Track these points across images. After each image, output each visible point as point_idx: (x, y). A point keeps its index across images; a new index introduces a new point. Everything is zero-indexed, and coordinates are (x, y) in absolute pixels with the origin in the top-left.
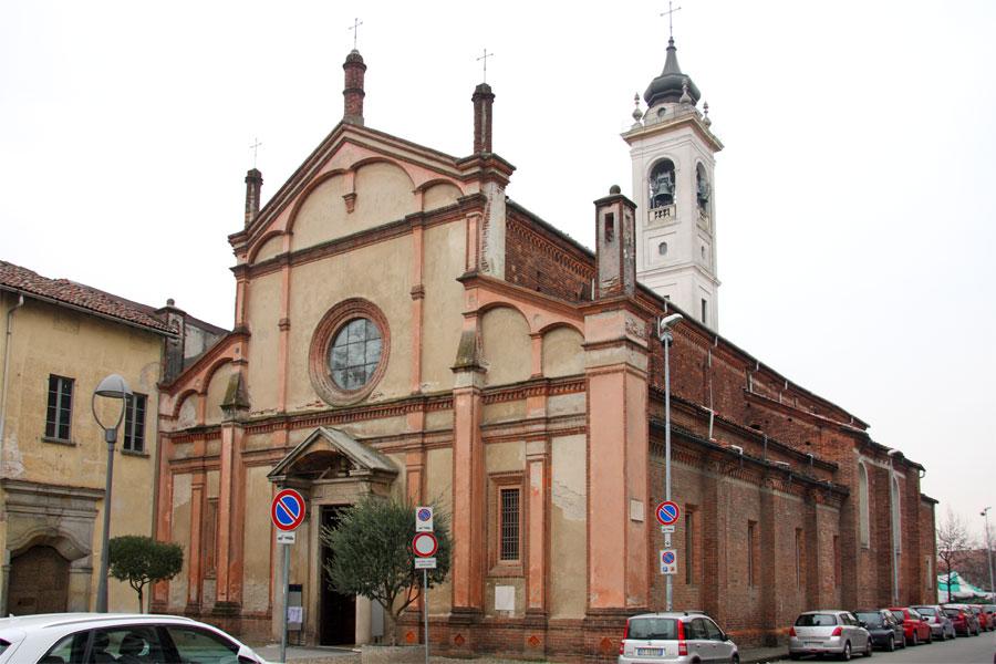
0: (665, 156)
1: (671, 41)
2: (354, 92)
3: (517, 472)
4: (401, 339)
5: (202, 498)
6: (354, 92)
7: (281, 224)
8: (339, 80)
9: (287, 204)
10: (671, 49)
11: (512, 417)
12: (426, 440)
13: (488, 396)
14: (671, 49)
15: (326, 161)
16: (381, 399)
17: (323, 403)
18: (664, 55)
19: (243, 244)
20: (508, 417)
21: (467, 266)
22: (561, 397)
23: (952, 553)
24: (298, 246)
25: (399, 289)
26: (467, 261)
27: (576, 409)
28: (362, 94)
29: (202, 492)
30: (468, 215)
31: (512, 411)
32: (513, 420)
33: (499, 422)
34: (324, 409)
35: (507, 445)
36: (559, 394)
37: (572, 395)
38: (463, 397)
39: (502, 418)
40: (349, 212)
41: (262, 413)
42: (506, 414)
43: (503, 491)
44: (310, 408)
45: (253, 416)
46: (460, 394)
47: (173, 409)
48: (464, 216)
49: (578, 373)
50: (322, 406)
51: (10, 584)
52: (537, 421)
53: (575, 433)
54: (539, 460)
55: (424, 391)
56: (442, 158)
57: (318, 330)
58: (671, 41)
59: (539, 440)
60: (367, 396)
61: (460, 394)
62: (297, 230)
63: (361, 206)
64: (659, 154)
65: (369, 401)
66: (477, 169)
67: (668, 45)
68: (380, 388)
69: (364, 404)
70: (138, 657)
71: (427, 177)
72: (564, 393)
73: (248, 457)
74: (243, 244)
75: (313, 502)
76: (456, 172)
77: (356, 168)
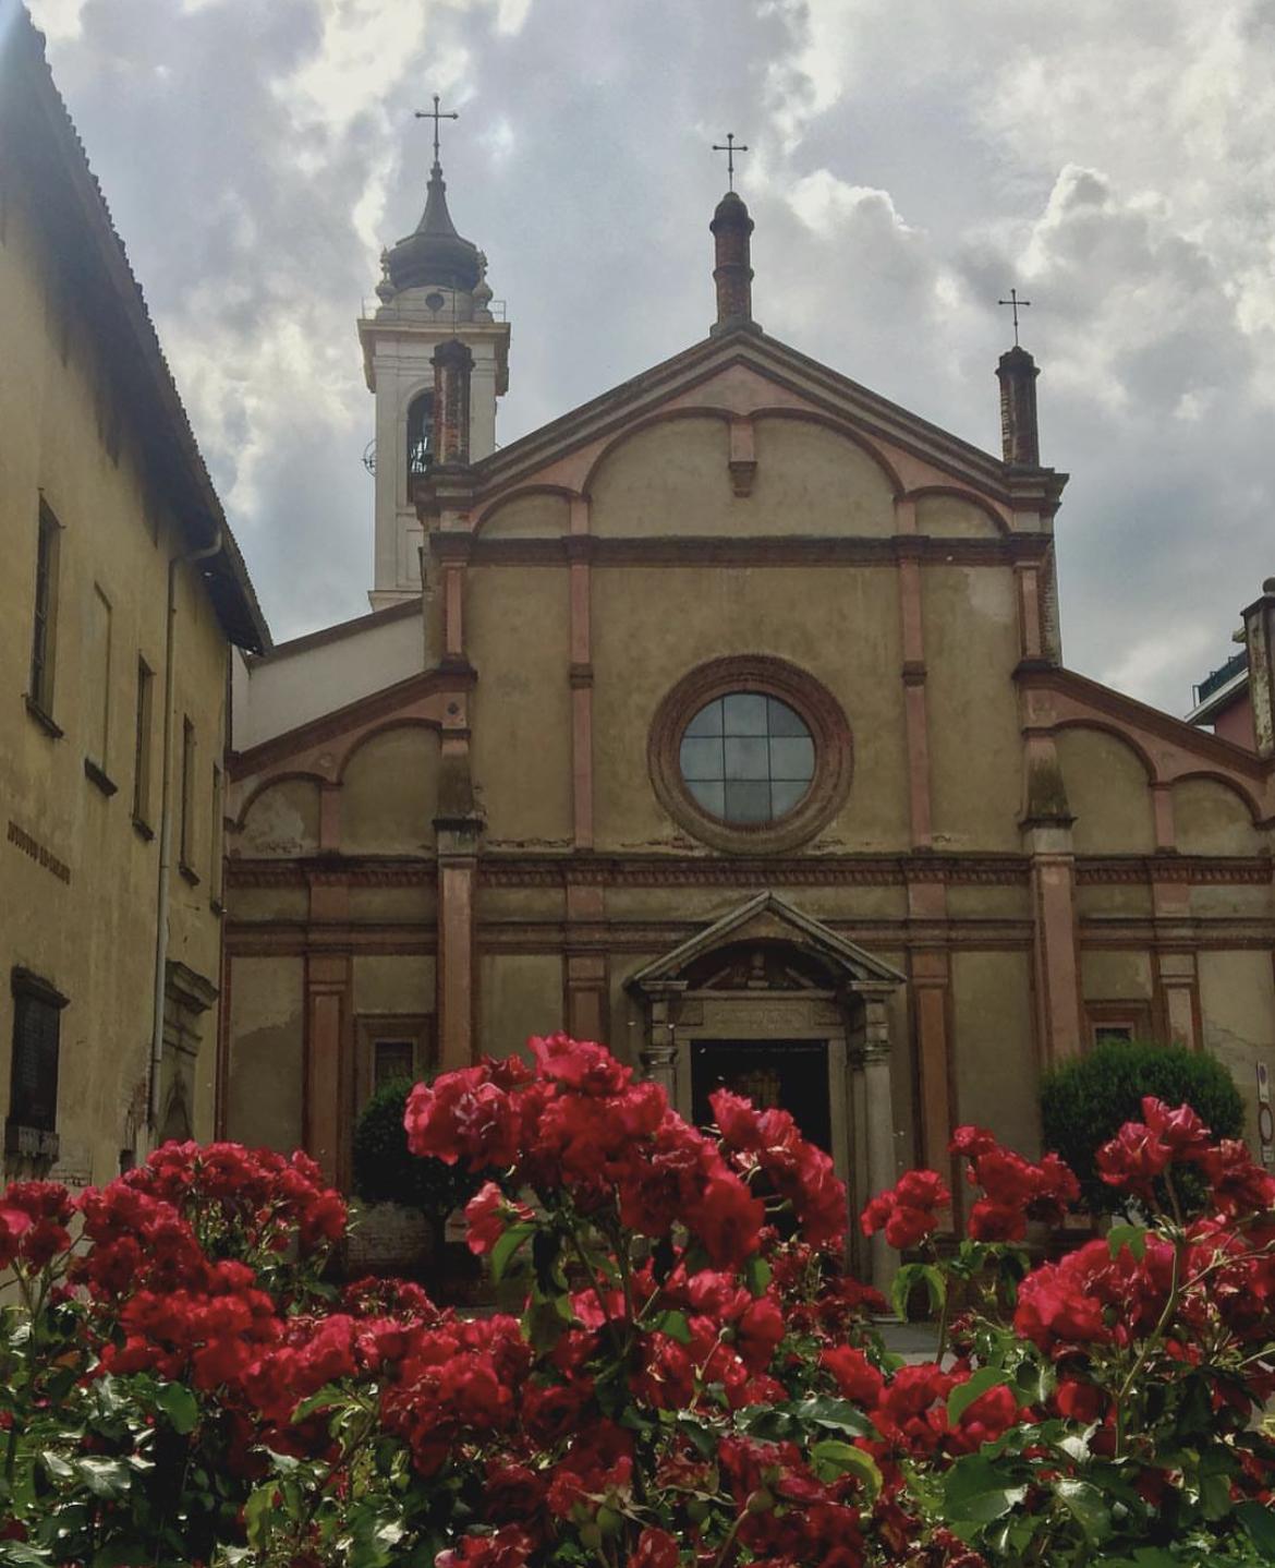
1: (437, 171)
2: (734, 274)
3: (1135, 1001)
4: (874, 747)
5: (341, 1013)
6: (734, 274)
7: (571, 473)
10: (437, 187)
12: (953, 934)
13: (1090, 869)
14: (437, 187)
16: (839, 850)
18: (423, 195)
22: (1207, 888)
23: (111, 1222)
24: (608, 528)
26: (1023, 641)
27: (1235, 911)
28: (750, 275)
29: (341, 1000)
30: (1019, 564)
31: (1119, 899)
32: (1122, 915)
33: (1095, 916)
34: (697, 853)
35: (1115, 956)
38: (1053, 869)
40: (737, 494)
41: (521, 845)
43: (1098, 1030)
44: (656, 849)
45: (495, 849)
47: (238, 809)
49: (1234, 854)
50: (691, 848)
55: (940, 846)
58: (437, 171)
59: (1185, 953)
60: (805, 842)
68: (834, 828)
73: (490, 934)
77: (756, 417)
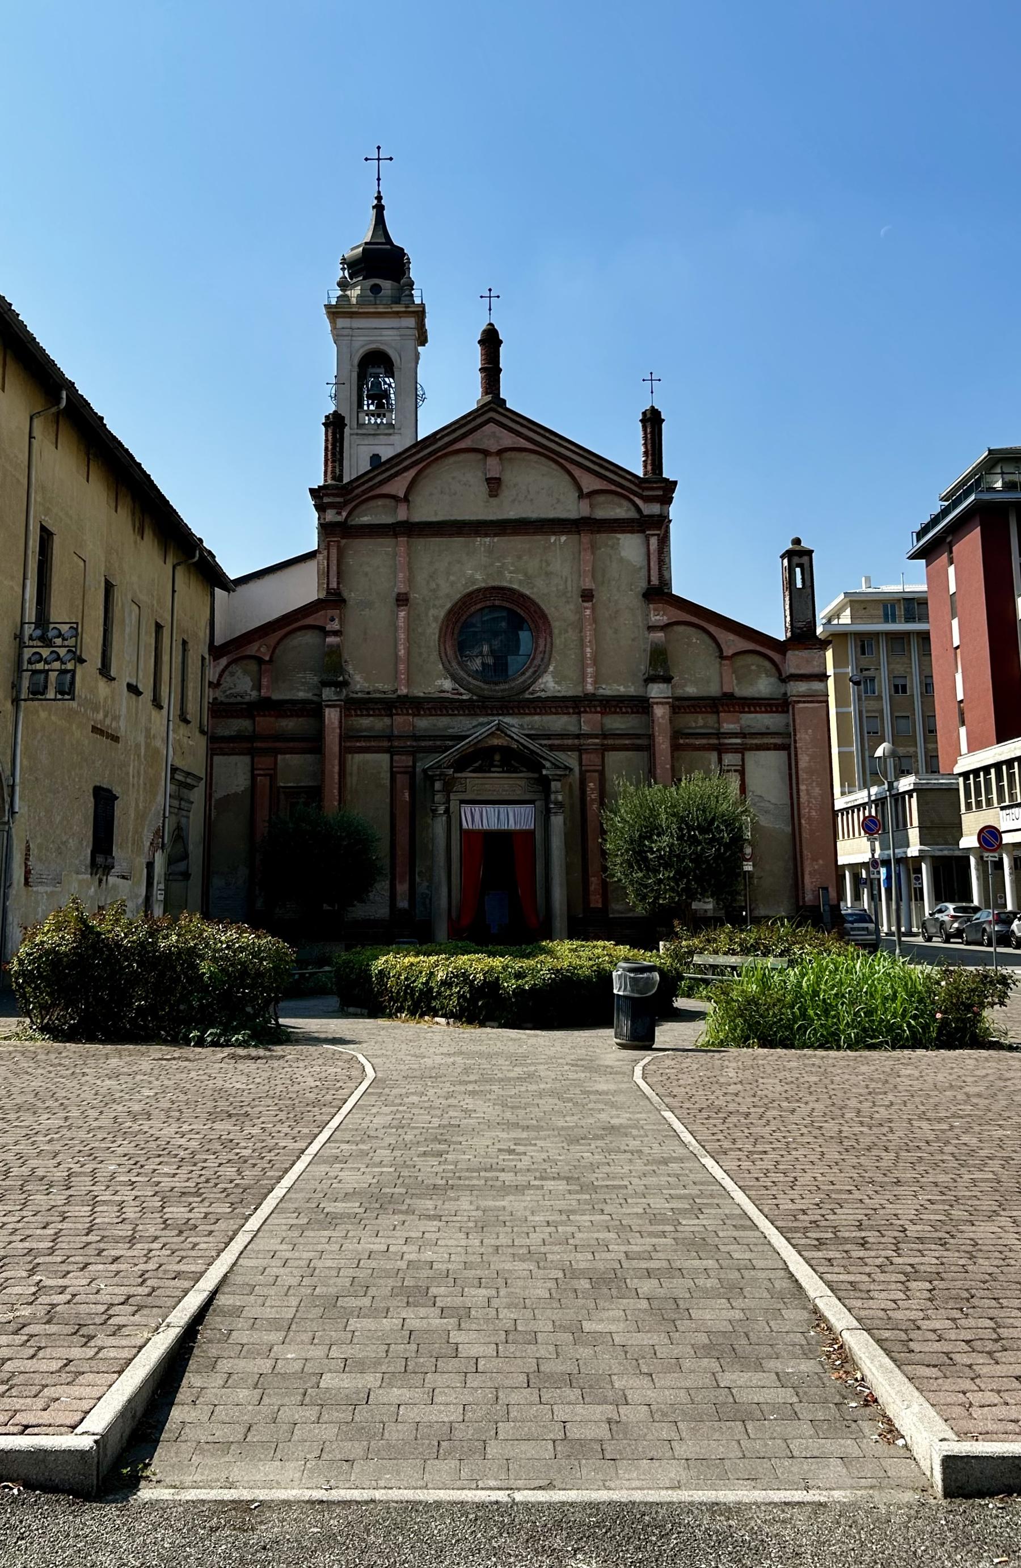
0: (382, 347)
1: (379, 198)
2: (491, 372)
6: (491, 372)
7: (398, 487)
8: (476, 353)
9: (406, 469)
10: (379, 208)
11: (701, 727)
14: (379, 208)
15: (464, 436)
17: (462, 691)
19: (338, 500)
20: (696, 728)
21: (649, 581)
22: (753, 715)
25: (561, 587)
31: (701, 722)
36: (750, 712)
37: (764, 715)
39: (690, 728)
41: (368, 693)
42: (694, 725)
46: (657, 703)
48: (643, 532)
50: (461, 694)
51: (567, 874)
52: (735, 735)
53: (769, 749)
54: (735, 771)
56: (620, 472)
57: (450, 611)
58: (379, 198)
61: (657, 703)
62: (416, 499)
63: (507, 493)
64: (372, 342)
65: (527, 696)
66: (660, 493)
67: (375, 202)
69: (516, 698)
70: (539, 947)
71: (598, 484)
72: (756, 712)
74: (338, 500)
75: (452, 797)
76: (640, 491)
